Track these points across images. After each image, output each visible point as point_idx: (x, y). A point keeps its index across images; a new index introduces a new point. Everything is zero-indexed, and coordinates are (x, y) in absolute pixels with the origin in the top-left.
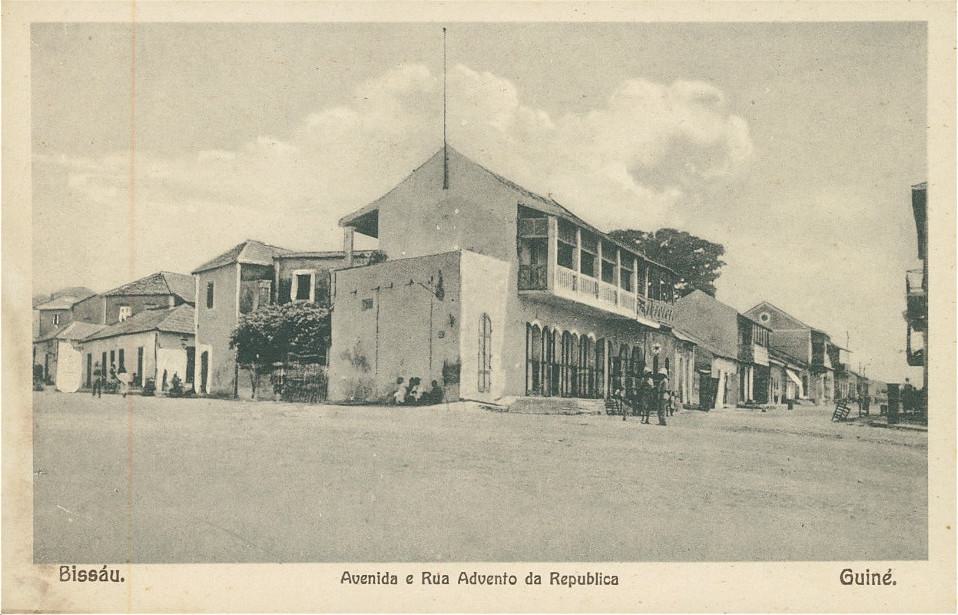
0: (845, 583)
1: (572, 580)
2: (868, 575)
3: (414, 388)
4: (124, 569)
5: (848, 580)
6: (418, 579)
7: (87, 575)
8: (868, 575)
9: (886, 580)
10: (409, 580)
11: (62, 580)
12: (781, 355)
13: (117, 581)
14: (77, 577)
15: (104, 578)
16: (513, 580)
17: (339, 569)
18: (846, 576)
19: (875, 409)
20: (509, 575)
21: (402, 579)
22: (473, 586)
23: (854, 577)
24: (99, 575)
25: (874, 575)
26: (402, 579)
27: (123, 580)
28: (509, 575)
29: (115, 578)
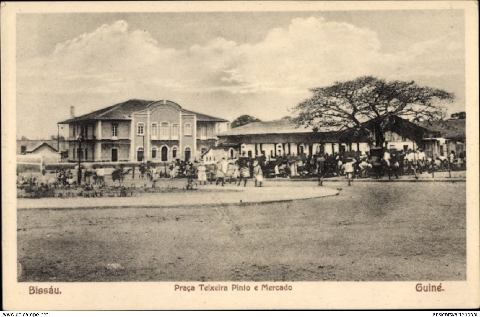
0: (418, 290)
1: (286, 288)
2: (430, 286)
3: (376, 109)
4: (445, 284)
5: (419, 289)
6: (260, 288)
7: (43, 290)
8: (430, 286)
9: (439, 289)
10: (256, 288)
11: (30, 293)
12: (115, 131)
13: (58, 293)
14: (38, 292)
15: (51, 292)
16: (290, 288)
17: (172, 284)
18: (419, 287)
19: (119, 194)
20: (246, 286)
21: (252, 288)
22: (426, 292)
23: (423, 287)
24: (49, 291)
25: (433, 287)
26: (252, 288)
27: (61, 293)
28: (246, 286)
29: (56, 291)
